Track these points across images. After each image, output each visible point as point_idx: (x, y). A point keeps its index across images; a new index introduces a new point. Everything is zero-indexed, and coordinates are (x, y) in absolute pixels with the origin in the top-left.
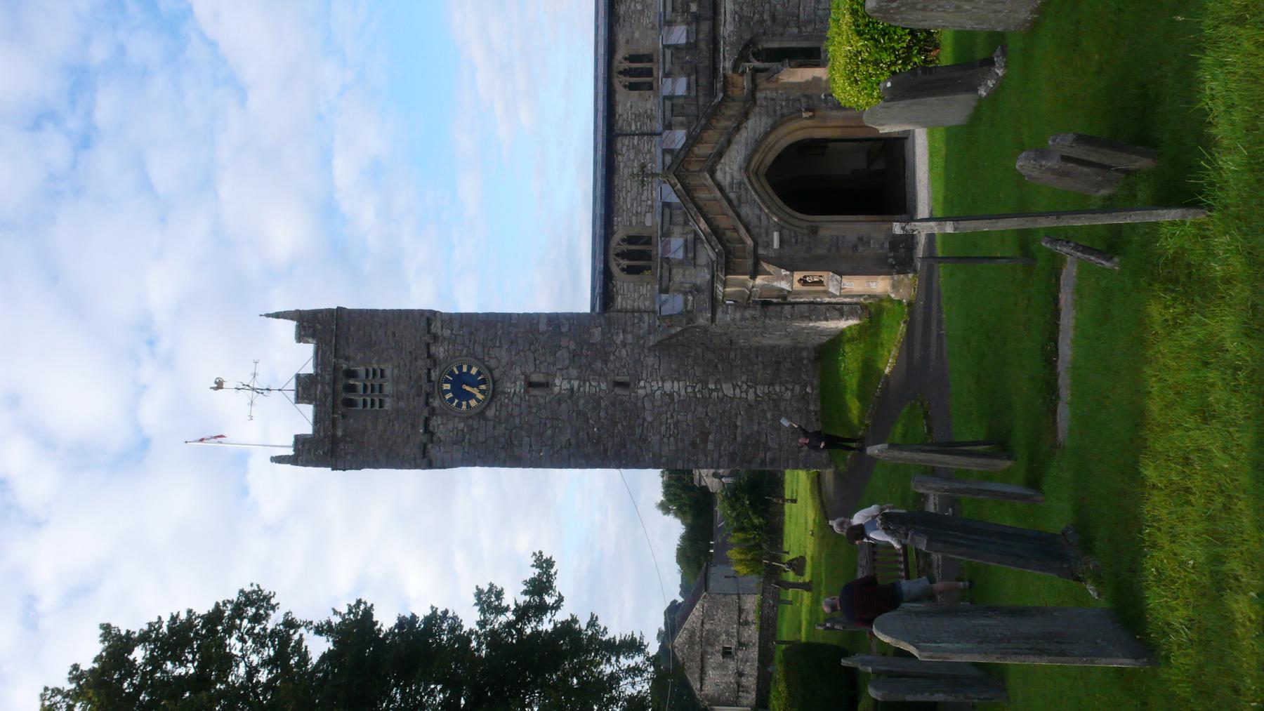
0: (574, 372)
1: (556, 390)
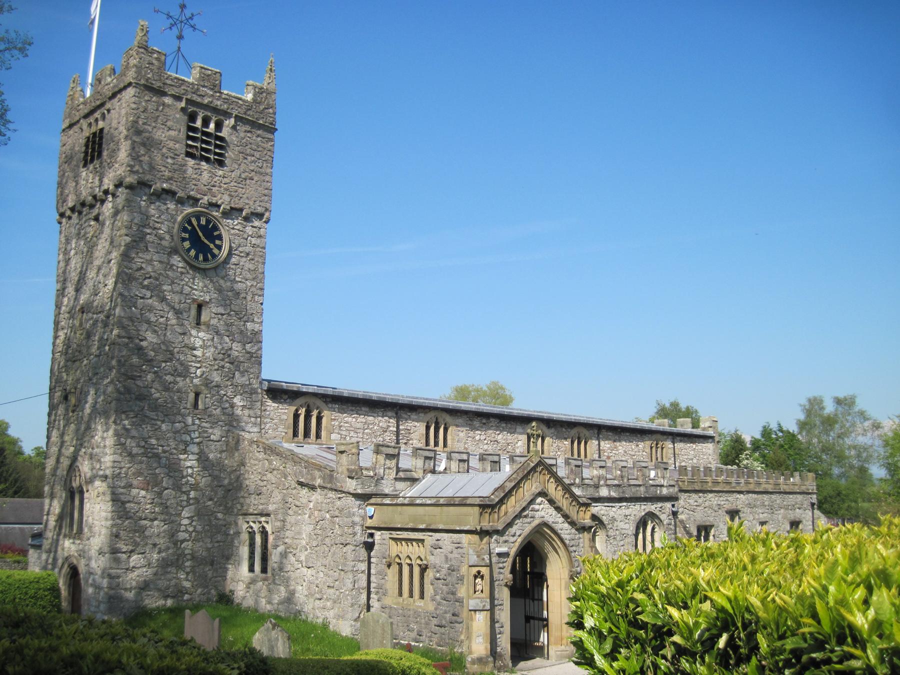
0: (210, 353)
1: (194, 332)
